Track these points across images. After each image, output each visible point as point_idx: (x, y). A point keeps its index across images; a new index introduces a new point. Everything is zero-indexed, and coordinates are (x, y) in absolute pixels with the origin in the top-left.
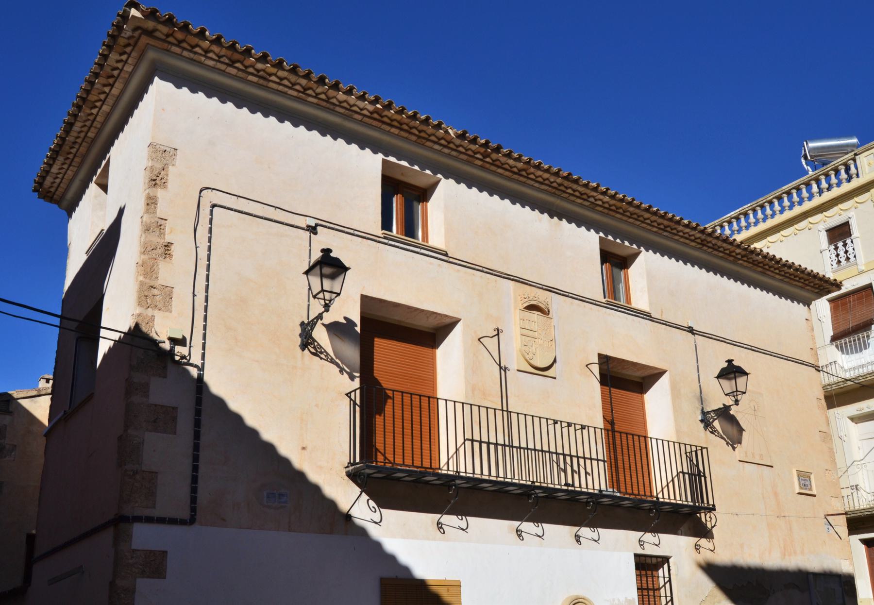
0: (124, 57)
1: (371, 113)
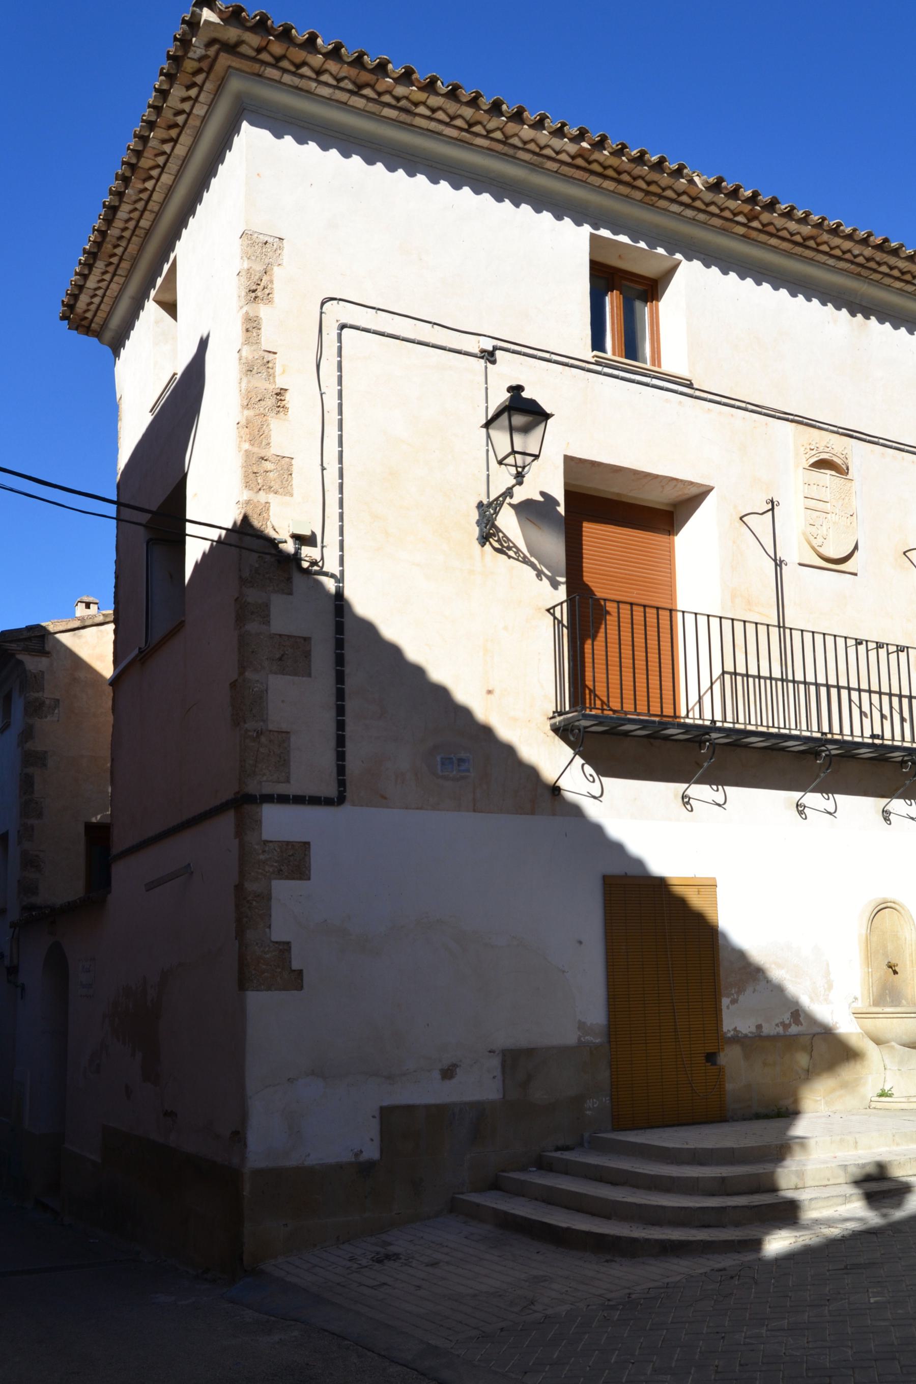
0: (193, 92)
1: (573, 158)
